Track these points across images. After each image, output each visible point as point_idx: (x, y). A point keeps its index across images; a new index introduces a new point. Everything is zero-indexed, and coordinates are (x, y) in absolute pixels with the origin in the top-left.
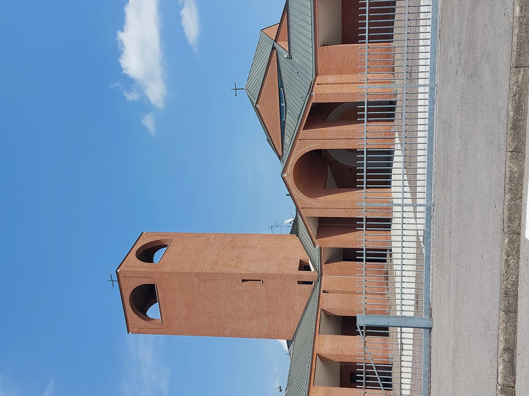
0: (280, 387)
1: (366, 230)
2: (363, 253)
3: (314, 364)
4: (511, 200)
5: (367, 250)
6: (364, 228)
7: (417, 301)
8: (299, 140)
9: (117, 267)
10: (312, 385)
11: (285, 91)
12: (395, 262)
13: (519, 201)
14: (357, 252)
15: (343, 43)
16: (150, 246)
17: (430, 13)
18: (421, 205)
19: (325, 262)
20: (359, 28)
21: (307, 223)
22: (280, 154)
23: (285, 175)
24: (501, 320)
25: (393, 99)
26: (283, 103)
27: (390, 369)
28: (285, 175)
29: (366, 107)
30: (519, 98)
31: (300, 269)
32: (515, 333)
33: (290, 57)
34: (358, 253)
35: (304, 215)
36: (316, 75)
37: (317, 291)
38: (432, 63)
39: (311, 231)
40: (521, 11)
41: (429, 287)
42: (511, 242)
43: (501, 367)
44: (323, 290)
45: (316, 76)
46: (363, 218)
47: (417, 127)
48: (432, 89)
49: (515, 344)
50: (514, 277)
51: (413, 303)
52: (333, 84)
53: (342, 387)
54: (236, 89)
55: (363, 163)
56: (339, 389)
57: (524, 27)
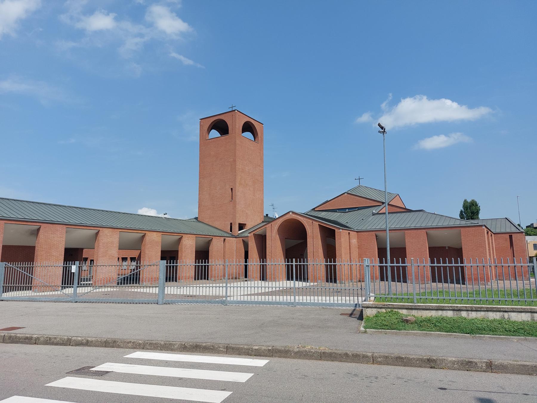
0: (167, 214)
1: (286, 265)
2: (203, 263)
3: (176, 234)
4: (161, 344)
5: (208, 266)
6: (262, 264)
7: (192, 296)
9: (239, 110)
10: (162, 233)
11: (355, 211)
12: (242, 283)
13: (159, 349)
14: (384, 259)
15: (430, 248)
16: (254, 130)
17: (302, 301)
18: (295, 298)
19: (244, 240)
20: (395, 259)
21: (263, 228)
22: (316, 210)
24: (102, 339)
25: (338, 281)
26: (348, 210)
27: (176, 281)
29: (333, 263)
30: (211, 349)
31: (240, 224)
32: (95, 346)
33: (374, 214)
34: (399, 259)
35: (267, 226)
36: (357, 232)
37: (226, 235)
38: (308, 303)
39: (253, 230)
40: (255, 350)
41: (181, 303)
42: (140, 344)
43: (80, 338)
44: (225, 239)
45: (357, 232)
46: (177, 264)
47: (316, 296)
48: (292, 303)
49: (90, 346)
50: (122, 346)
51: (191, 294)
52: (350, 242)
53: (65, 253)
55: (383, 263)
56: (160, 250)
57: (247, 351)
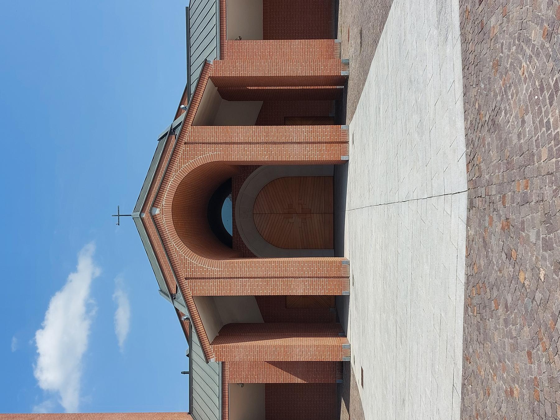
8: (185, 143)
23: (157, 211)
28: (157, 211)
35: (189, 293)
54: (119, 216)
